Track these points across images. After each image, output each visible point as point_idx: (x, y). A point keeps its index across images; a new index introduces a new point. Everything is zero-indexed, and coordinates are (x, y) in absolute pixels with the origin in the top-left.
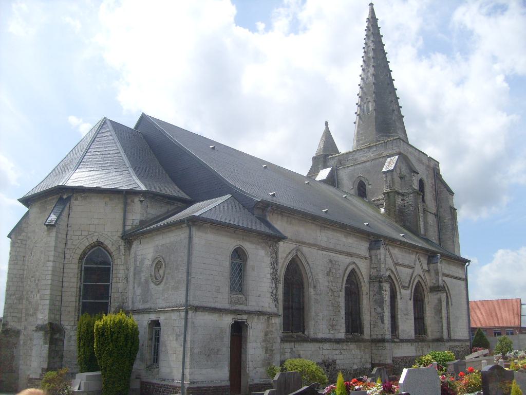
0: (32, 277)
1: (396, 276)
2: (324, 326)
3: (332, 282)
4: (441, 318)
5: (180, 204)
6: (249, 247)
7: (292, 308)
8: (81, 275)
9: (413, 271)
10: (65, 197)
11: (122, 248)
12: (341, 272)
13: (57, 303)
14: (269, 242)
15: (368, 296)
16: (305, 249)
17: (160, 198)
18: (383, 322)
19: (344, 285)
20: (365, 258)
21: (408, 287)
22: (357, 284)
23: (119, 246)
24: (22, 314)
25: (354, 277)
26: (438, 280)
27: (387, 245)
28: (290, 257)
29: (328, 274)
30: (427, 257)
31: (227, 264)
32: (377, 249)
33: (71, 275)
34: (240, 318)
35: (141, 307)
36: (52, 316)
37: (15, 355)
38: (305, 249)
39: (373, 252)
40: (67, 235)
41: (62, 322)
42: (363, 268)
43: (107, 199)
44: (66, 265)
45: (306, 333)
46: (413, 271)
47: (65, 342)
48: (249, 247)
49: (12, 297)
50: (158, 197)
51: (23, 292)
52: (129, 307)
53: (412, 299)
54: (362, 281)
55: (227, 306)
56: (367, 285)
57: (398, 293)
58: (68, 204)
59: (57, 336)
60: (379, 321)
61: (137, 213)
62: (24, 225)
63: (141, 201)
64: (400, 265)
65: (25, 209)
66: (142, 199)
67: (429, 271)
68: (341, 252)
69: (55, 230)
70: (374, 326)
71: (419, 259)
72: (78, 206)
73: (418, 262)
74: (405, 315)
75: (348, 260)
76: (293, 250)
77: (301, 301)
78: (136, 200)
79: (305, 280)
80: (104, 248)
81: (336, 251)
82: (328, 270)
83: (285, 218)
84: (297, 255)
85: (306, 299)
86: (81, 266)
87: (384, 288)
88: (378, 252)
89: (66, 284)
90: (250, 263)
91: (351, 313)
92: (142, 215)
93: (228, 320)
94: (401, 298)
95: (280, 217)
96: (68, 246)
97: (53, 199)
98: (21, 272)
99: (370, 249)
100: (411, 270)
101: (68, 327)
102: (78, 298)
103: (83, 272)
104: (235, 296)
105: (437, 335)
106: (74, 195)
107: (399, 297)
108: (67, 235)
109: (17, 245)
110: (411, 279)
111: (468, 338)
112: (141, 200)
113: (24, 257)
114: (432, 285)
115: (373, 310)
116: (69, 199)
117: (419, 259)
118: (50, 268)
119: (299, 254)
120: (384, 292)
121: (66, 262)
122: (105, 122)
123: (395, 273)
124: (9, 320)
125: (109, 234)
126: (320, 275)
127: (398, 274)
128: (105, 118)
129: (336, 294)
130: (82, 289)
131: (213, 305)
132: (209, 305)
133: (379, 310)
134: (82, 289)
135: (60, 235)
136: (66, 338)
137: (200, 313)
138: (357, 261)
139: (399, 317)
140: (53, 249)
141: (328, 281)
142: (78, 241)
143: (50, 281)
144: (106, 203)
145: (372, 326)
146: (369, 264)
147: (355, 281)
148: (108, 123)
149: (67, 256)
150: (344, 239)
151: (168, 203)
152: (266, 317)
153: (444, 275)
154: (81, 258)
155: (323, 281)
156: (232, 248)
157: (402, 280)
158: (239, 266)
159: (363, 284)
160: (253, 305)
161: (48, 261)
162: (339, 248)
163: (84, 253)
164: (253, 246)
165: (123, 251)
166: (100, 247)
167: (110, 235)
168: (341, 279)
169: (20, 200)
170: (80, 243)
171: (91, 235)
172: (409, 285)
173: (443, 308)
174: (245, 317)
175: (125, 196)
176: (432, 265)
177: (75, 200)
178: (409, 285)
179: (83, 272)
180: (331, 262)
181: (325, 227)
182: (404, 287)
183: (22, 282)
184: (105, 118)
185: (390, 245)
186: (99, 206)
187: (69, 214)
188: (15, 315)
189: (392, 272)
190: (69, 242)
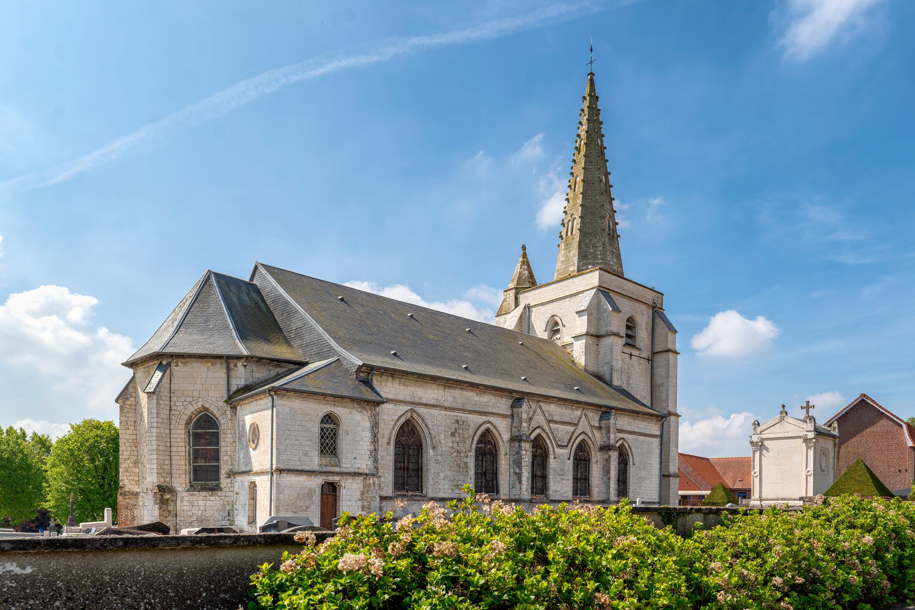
0: (144, 442)
1: (550, 435)
2: (447, 486)
3: (458, 443)
4: (609, 479)
5: (292, 366)
6: (340, 411)
7: (408, 469)
8: (189, 439)
9: (575, 430)
10: (164, 363)
11: (228, 412)
12: (471, 432)
13: (166, 467)
14: (367, 407)
15: (508, 456)
16: (422, 410)
17: (266, 361)
18: (520, 483)
19: (474, 446)
20: (505, 416)
21: (566, 446)
22: (495, 444)
23: (225, 411)
24: (139, 477)
25: (490, 437)
26: (609, 438)
27: (539, 401)
28: (403, 420)
29: (453, 434)
30: (600, 413)
31: (316, 430)
32: (519, 407)
33: (179, 440)
34: (331, 479)
35: (244, 469)
36: (162, 479)
37: (135, 515)
38: (422, 410)
39: (515, 410)
40: (170, 401)
41: (173, 484)
42: (503, 430)
43: (210, 364)
44: (173, 431)
45: (424, 492)
46: (575, 430)
47: (178, 503)
48: (340, 411)
49: (126, 461)
50: (264, 360)
51: (137, 456)
52: (62, 474)
53: (572, 458)
54: (500, 440)
55: (316, 467)
56: (507, 445)
57: (551, 452)
58: (168, 371)
59: (167, 496)
60: (517, 482)
61: (241, 376)
62: (131, 390)
63: (245, 366)
64: (555, 422)
65: (130, 372)
66: (245, 364)
67: (600, 428)
68: (471, 412)
69: (155, 397)
70: (512, 487)
71: (586, 415)
72: (179, 370)
73: (583, 418)
74: (560, 475)
75: (481, 419)
76: (406, 412)
77: (420, 461)
78: (240, 364)
79: (423, 441)
80: (210, 413)
81: (464, 411)
82: (453, 430)
83: (398, 380)
84: (412, 417)
85: (424, 460)
86: (189, 432)
87: (523, 448)
88: (520, 410)
89: (174, 449)
90: (343, 428)
91: (485, 473)
92: (246, 379)
93: (316, 482)
94: (555, 458)
95: (390, 379)
96: (174, 412)
97: (155, 364)
98: (134, 437)
99: (513, 406)
100: (573, 428)
101: (180, 489)
102: (187, 462)
103: (191, 437)
104: (327, 460)
105: (603, 497)
106: (174, 361)
107: (552, 457)
108: (170, 401)
109: (126, 410)
110: (571, 437)
111: (658, 501)
112: (244, 364)
113: (135, 422)
114: (602, 443)
115: (512, 470)
116: (169, 364)
117: (586, 415)
118: (154, 434)
119: (415, 415)
120: (524, 452)
121: (172, 428)
122: (209, 277)
123: (548, 431)
124: (126, 484)
125: (214, 399)
126: (442, 436)
127: (552, 433)
128: (209, 271)
129: (462, 455)
130: (191, 453)
131: (300, 468)
132: (296, 468)
133: (517, 470)
134: (191, 453)
135: (161, 402)
136: (179, 499)
137: (285, 475)
138: (492, 419)
139: (551, 477)
140: (155, 416)
141: (452, 442)
142: (182, 407)
143: (155, 446)
144: (208, 369)
145: (511, 486)
146: (510, 424)
147: (492, 441)
148: (213, 279)
149: (173, 422)
150: (477, 398)
151: (277, 366)
152: (362, 478)
153: (620, 431)
154: (187, 424)
155: (445, 442)
156: (321, 415)
157: (557, 439)
158: (332, 431)
159: (501, 444)
160: (347, 465)
161: (152, 427)
162: (468, 407)
163: (190, 418)
164: (347, 411)
165: (230, 416)
166: (207, 413)
167: (215, 400)
168: (471, 440)
169: (125, 364)
170: (186, 410)
171: (196, 401)
172: (568, 444)
173: (612, 468)
174: (337, 478)
175: (227, 361)
176: (603, 422)
177: (176, 366)
178: (568, 444)
179: (191, 437)
180: (457, 422)
181: (450, 387)
182: (560, 446)
183: (136, 447)
184: (209, 271)
185: (543, 402)
186: (201, 370)
187: (171, 381)
188: (131, 478)
189: (544, 430)
190: (173, 408)
